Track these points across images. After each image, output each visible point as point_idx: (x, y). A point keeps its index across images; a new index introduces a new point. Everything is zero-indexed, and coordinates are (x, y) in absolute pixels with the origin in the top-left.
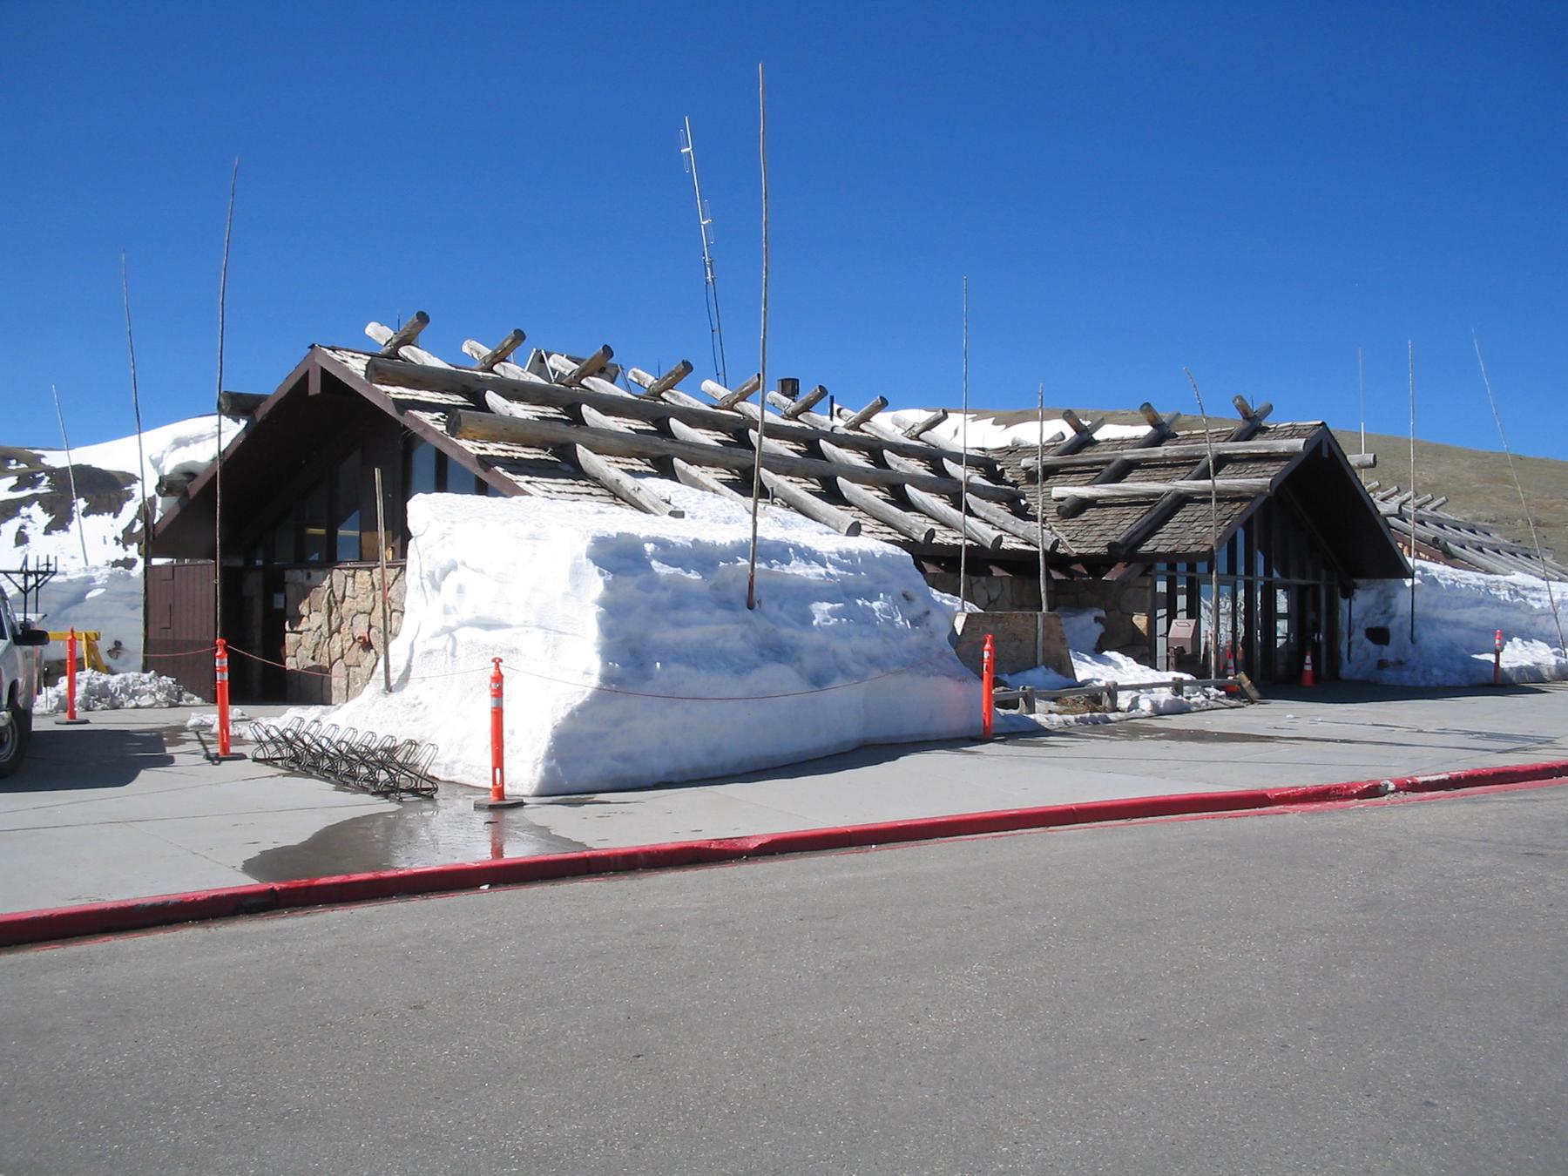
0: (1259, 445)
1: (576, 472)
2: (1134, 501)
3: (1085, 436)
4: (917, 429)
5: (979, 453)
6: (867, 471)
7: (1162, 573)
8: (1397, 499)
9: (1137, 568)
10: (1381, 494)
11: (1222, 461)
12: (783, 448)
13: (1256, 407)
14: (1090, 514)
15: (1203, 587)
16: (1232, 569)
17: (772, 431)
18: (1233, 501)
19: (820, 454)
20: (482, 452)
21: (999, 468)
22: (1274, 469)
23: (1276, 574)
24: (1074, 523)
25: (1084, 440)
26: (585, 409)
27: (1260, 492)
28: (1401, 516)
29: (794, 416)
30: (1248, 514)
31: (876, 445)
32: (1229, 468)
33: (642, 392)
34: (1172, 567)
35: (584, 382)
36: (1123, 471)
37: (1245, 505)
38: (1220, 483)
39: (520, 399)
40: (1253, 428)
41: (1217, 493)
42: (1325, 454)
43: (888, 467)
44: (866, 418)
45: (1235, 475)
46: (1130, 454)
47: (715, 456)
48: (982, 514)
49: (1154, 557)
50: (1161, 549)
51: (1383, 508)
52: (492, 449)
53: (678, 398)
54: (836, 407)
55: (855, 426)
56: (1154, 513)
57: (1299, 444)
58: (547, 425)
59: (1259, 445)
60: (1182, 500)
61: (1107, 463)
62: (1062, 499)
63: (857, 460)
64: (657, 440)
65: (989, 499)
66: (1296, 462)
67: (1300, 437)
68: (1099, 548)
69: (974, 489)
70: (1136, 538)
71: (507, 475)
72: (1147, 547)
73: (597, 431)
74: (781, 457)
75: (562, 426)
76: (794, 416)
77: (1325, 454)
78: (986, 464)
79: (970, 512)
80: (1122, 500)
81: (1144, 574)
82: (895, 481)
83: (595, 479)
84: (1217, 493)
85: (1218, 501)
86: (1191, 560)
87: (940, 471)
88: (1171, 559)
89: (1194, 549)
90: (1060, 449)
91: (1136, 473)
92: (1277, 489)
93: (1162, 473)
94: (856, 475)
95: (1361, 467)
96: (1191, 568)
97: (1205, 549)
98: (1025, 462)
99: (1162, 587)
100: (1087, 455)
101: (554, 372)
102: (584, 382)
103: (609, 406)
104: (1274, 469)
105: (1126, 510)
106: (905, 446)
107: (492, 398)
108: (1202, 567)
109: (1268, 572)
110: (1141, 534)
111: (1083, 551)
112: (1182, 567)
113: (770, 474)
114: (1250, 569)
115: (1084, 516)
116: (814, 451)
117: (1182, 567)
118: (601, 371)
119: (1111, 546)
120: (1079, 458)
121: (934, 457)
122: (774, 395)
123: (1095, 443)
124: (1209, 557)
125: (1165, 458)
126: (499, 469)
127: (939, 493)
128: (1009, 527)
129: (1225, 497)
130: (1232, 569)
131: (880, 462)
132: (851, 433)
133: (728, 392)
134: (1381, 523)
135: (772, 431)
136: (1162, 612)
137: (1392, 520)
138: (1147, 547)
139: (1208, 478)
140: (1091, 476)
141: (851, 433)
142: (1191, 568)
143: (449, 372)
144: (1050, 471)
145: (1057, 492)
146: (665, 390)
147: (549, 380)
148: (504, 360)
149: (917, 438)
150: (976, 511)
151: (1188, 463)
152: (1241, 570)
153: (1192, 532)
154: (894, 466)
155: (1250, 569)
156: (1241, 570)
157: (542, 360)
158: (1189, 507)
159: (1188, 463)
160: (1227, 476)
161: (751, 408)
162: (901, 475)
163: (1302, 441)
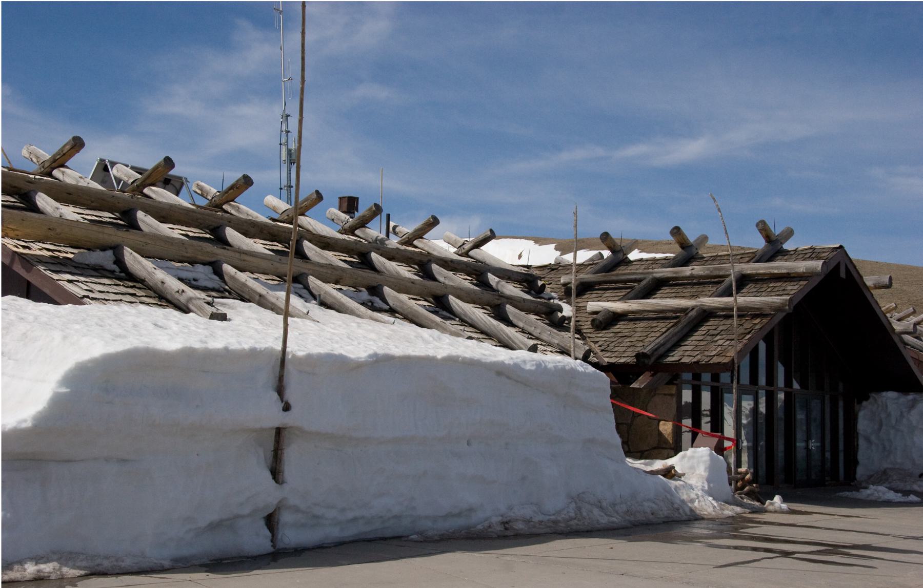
0: (779, 266)
1: (124, 275)
2: (661, 315)
3: (621, 256)
4: (467, 247)
5: (523, 270)
6: (413, 282)
7: (687, 382)
8: (914, 319)
9: (664, 376)
10: (897, 315)
11: (743, 281)
12: (334, 258)
13: (777, 230)
14: (621, 327)
15: (726, 396)
16: (754, 379)
17: (325, 243)
18: (755, 316)
19: (371, 266)
20: (26, 251)
21: (540, 283)
22: (793, 288)
23: (796, 386)
24: (604, 336)
25: (620, 260)
26: (140, 215)
27: (778, 309)
28: (914, 333)
29: (351, 231)
30: (768, 329)
31: (425, 259)
32: (751, 287)
33: (203, 202)
34: (697, 377)
35: (146, 191)
36: (654, 287)
37: (765, 321)
38: (743, 300)
39: (75, 203)
40: (774, 249)
41: (739, 309)
42: (843, 274)
43: (435, 279)
44: (420, 234)
45: (758, 293)
46: (667, 272)
47: (264, 264)
48: (521, 324)
49: (679, 367)
50: (686, 360)
51: (898, 327)
52: (37, 249)
53: (238, 209)
54: (392, 224)
55: (409, 242)
56: (680, 326)
57: (817, 265)
58: (95, 228)
59: (779, 266)
60: (706, 315)
61: (640, 281)
62: (596, 313)
63: (405, 272)
64: (209, 247)
65: (529, 311)
66: (817, 280)
67: (819, 258)
68: (627, 358)
69: (512, 301)
70: (662, 350)
71: (48, 273)
72: (673, 358)
73: (241, 252)
74: (331, 267)
75: (111, 230)
76: (351, 231)
77: (843, 274)
78: (528, 279)
79: (510, 324)
80: (651, 315)
81: (670, 383)
82: (439, 292)
83: (142, 281)
84: (739, 309)
85: (739, 316)
86: (716, 370)
87: (483, 283)
88: (696, 369)
89: (716, 360)
90: (597, 268)
91: (666, 290)
92: (796, 307)
93: (689, 290)
94: (402, 286)
95: (878, 287)
96: (715, 378)
97: (726, 360)
98: (563, 280)
99: (687, 396)
100: (622, 272)
101: (118, 181)
102: (146, 191)
103: (165, 214)
104: (793, 288)
105: (654, 323)
106: (452, 261)
107: (43, 201)
108: (725, 377)
109: (788, 383)
110: (668, 346)
111: (613, 360)
112: (706, 377)
113: (319, 283)
114: (771, 379)
115: (616, 329)
116: (365, 262)
117: (706, 377)
118: (167, 183)
119: (638, 356)
120: (613, 276)
121: (479, 272)
122: (335, 211)
123: (630, 262)
124: (730, 367)
125: (692, 277)
126: (42, 268)
127: (482, 304)
128: (545, 337)
129: (745, 313)
130: (754, 379)
131: (428, 275)
132: (465, 259)
133: (288, 207)
134: (896, 340)
135: (325, 243)
136: (687, 422)
137: (907, 338)
138: (673, 358)
139: (731, 295)
140: (624, 292)
141: (403, 247)
142: (715, 378)
143: (97, 192)
144: (585, 288)
145: (593, 305)
146: (227, 202)
147: (110, 186)
148: (63, 166)
149: (466, 254)
150: (515, 321)
151: (713, 281)
152: (762, 380)
153: (715, 346)
154: (441, 279)
155: (771, 379)
156: (762, 380)
157: (106, 169)
158: (712, 322)
159: (713, 281)
160: (749, 294)
161: (307, 221)
162: (446, 286)
163: (820, 263)
